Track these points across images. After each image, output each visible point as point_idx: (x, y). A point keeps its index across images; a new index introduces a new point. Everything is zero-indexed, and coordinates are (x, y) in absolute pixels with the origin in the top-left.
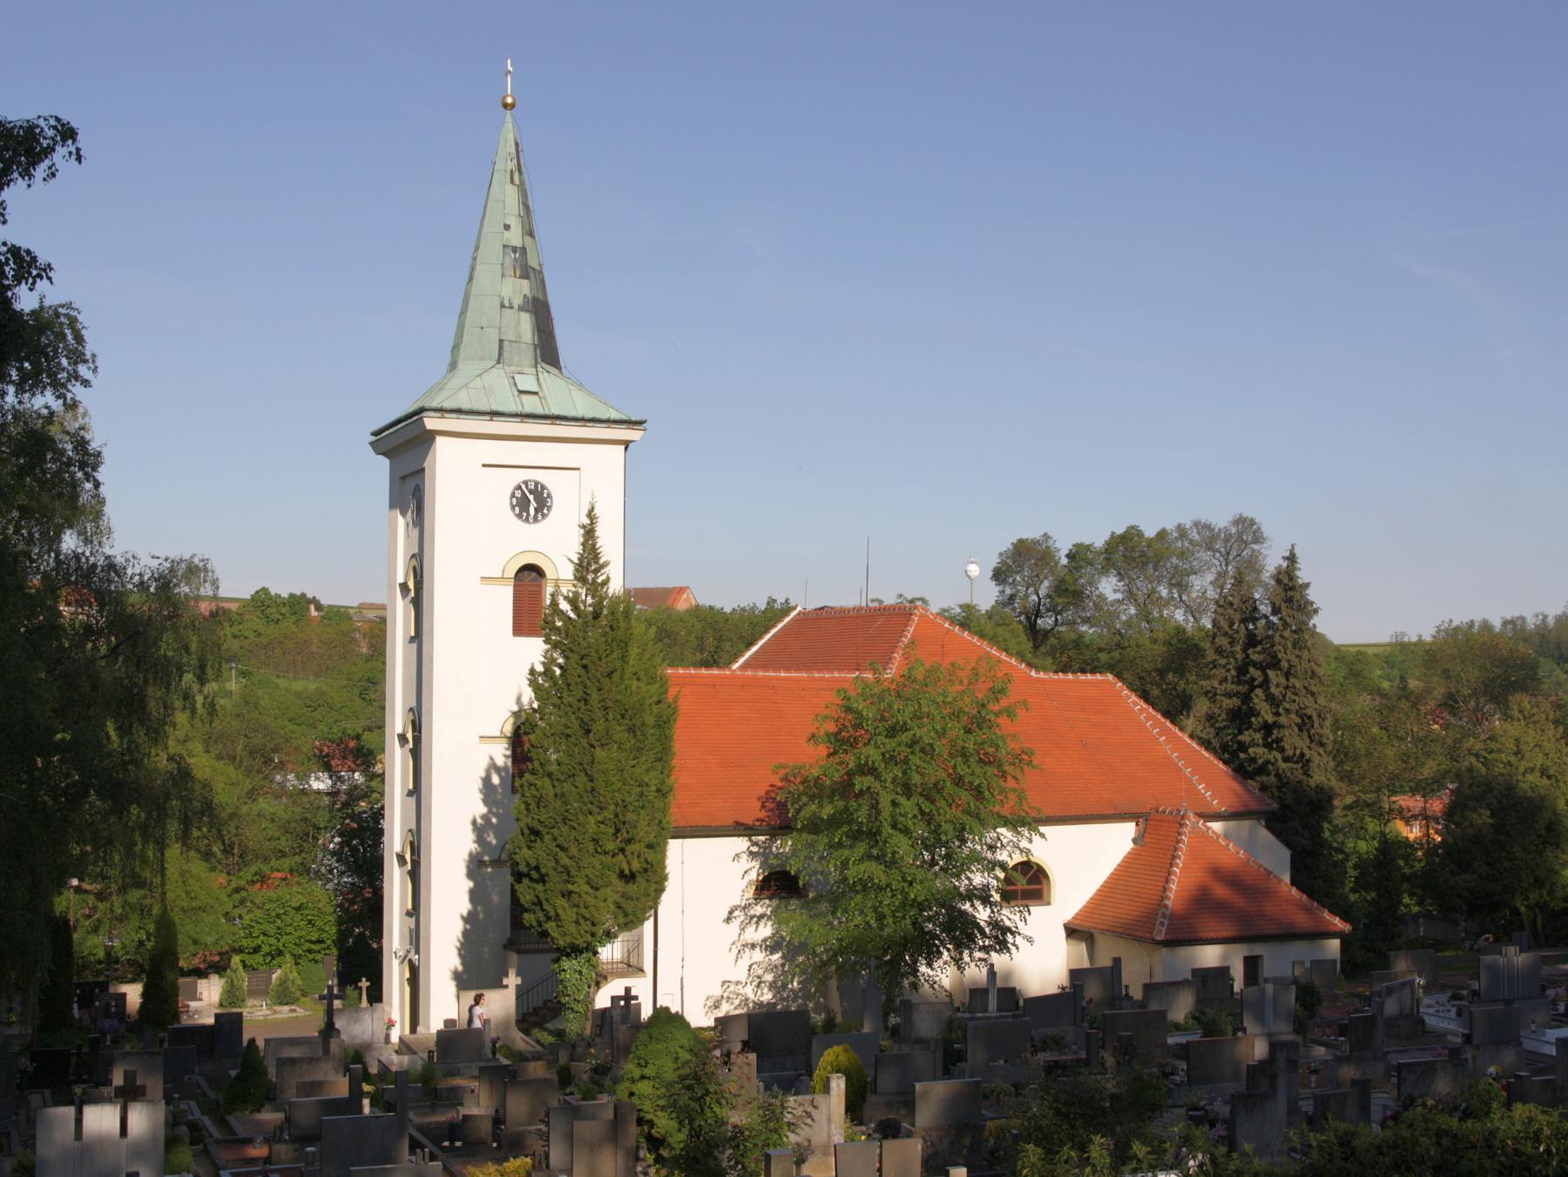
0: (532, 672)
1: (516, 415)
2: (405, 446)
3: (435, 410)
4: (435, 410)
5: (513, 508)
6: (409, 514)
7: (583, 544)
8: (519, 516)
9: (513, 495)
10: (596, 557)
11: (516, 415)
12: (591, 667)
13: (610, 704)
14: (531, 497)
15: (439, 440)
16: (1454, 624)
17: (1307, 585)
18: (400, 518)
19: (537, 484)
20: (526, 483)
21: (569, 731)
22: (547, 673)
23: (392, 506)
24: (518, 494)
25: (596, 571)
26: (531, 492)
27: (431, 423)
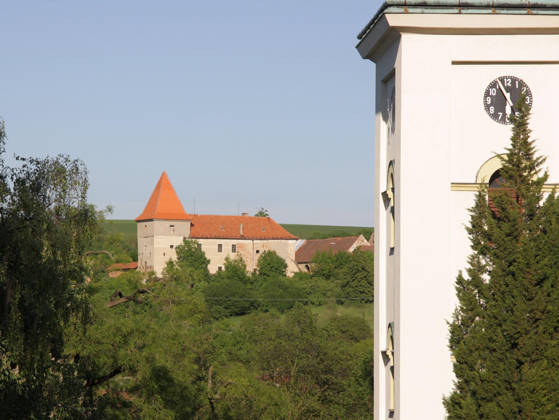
0: (460, 281)
1: (488, 7)
2: (380, 44)
3: (398, 5)
4: (398, 5)
5: (487, 107)
6: (389, 122)
7: (513, 139)
8: (495, 116)
9: (487, 94)
10: (528, 155)
11: (488, 7)
12: (518, 275)
13: (538, 315)
14: (508, 95)
15: (405, 38)
16: (470, 226)
17: (528, 124)
18: (383, 123)
19: (514, 80)
20: (502, 80)
21: (493, 345)
22: (476, 282)
23: (377, 111)
24: (493, 92)
25: (532, 168)
26: (508, 89)
27: (394, 19)
